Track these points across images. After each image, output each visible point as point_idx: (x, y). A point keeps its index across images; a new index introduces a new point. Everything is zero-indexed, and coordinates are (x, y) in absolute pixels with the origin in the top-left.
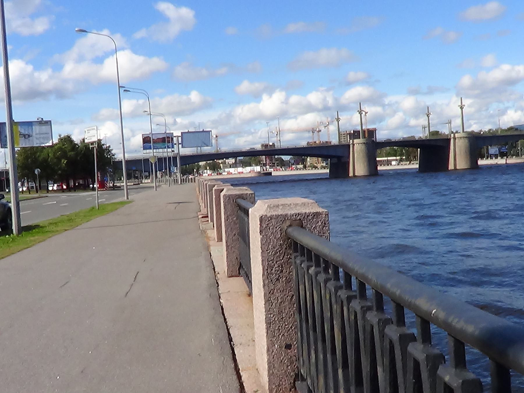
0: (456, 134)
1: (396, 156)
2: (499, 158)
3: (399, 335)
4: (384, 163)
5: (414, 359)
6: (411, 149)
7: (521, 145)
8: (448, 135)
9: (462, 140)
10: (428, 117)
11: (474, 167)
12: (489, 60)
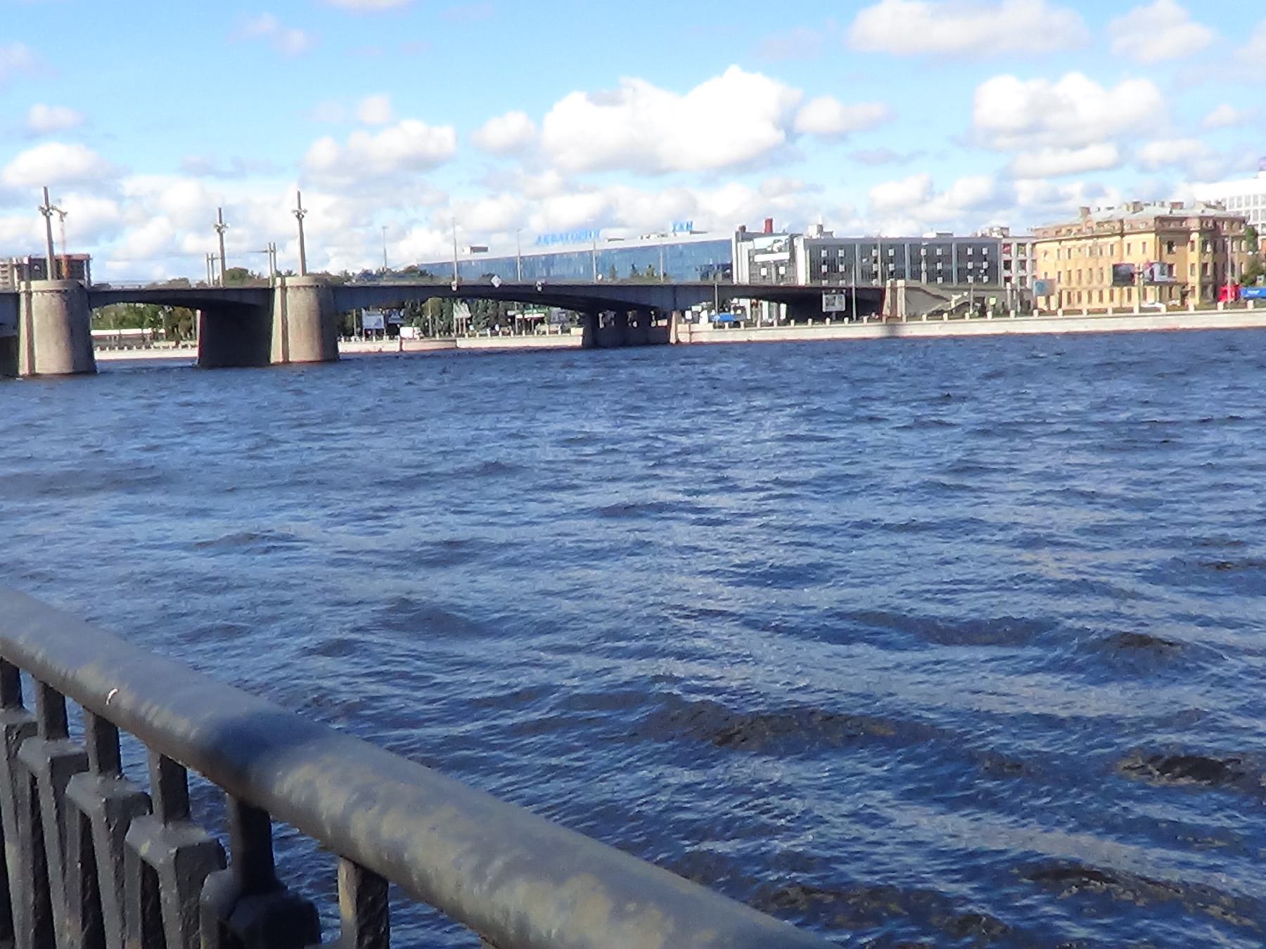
0: (287, 279)
1: (140, 325)
2: (386, 338)
3: (49, 759)
4: (113, 343)
5: (81, 811)
6: (179, 310)
7: (433, 309)
8: (268, 279)
9: (301, 294)
10: (221, 235)
11: (330, 357)
12: (375, 107)
